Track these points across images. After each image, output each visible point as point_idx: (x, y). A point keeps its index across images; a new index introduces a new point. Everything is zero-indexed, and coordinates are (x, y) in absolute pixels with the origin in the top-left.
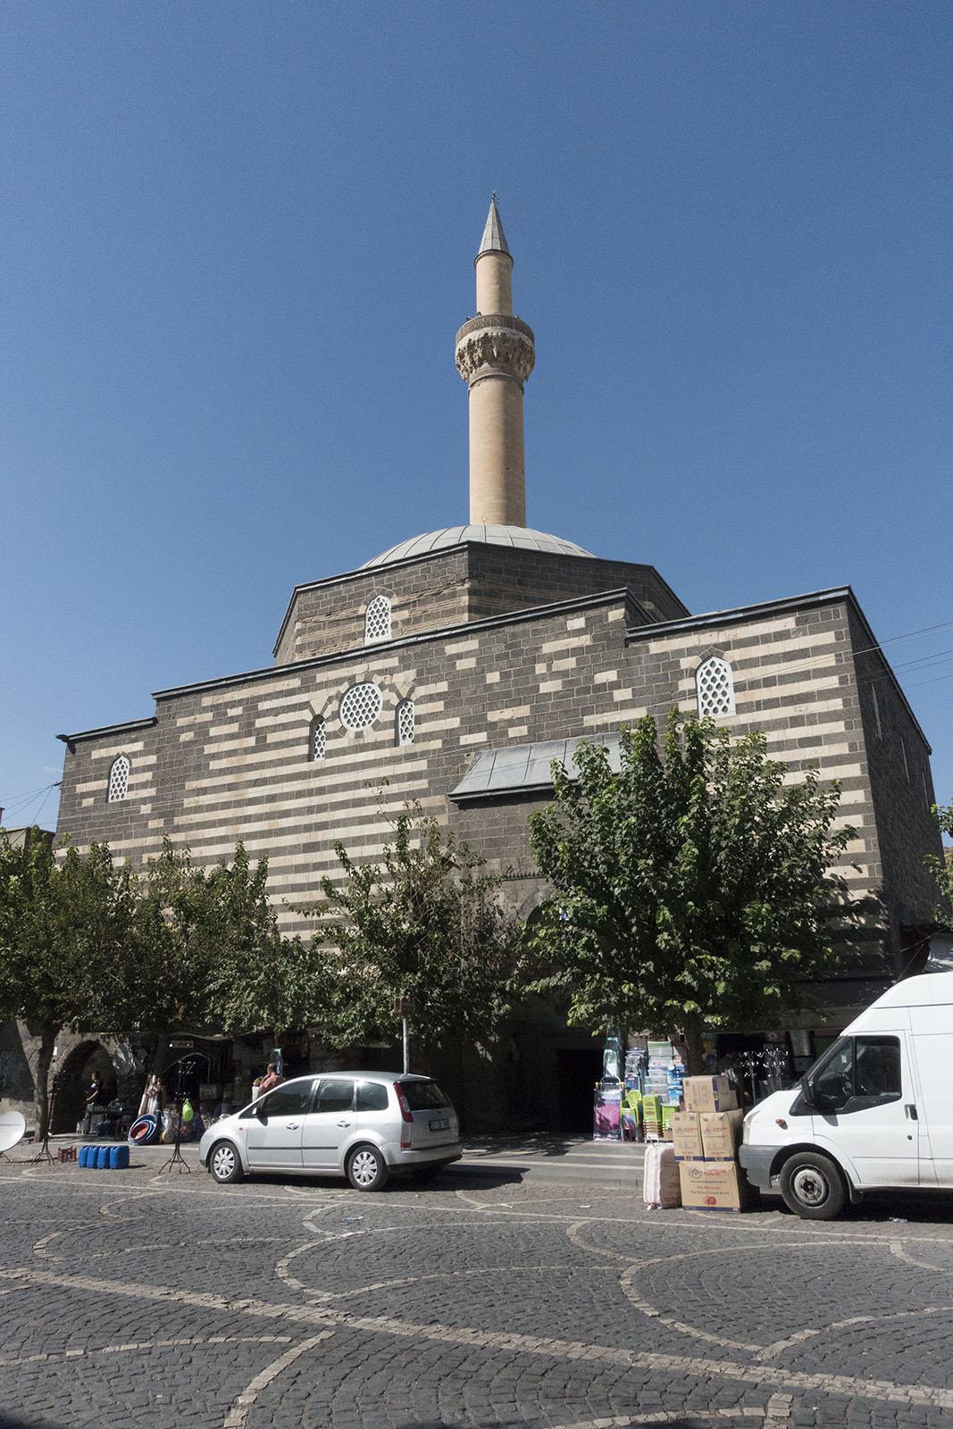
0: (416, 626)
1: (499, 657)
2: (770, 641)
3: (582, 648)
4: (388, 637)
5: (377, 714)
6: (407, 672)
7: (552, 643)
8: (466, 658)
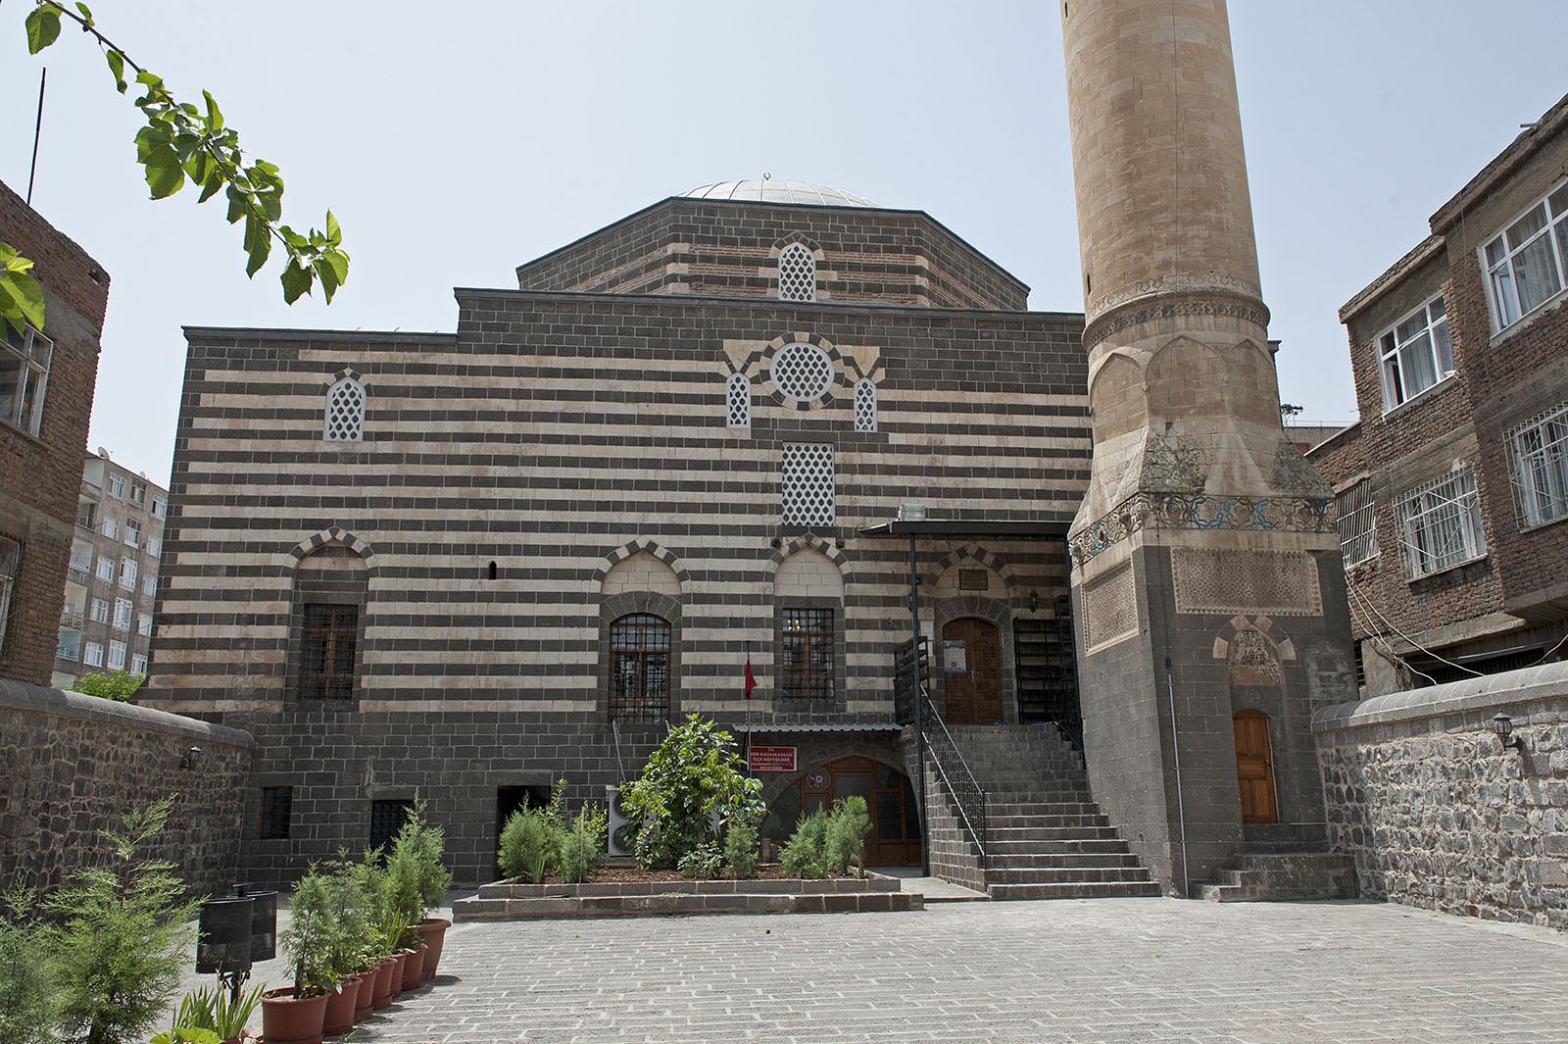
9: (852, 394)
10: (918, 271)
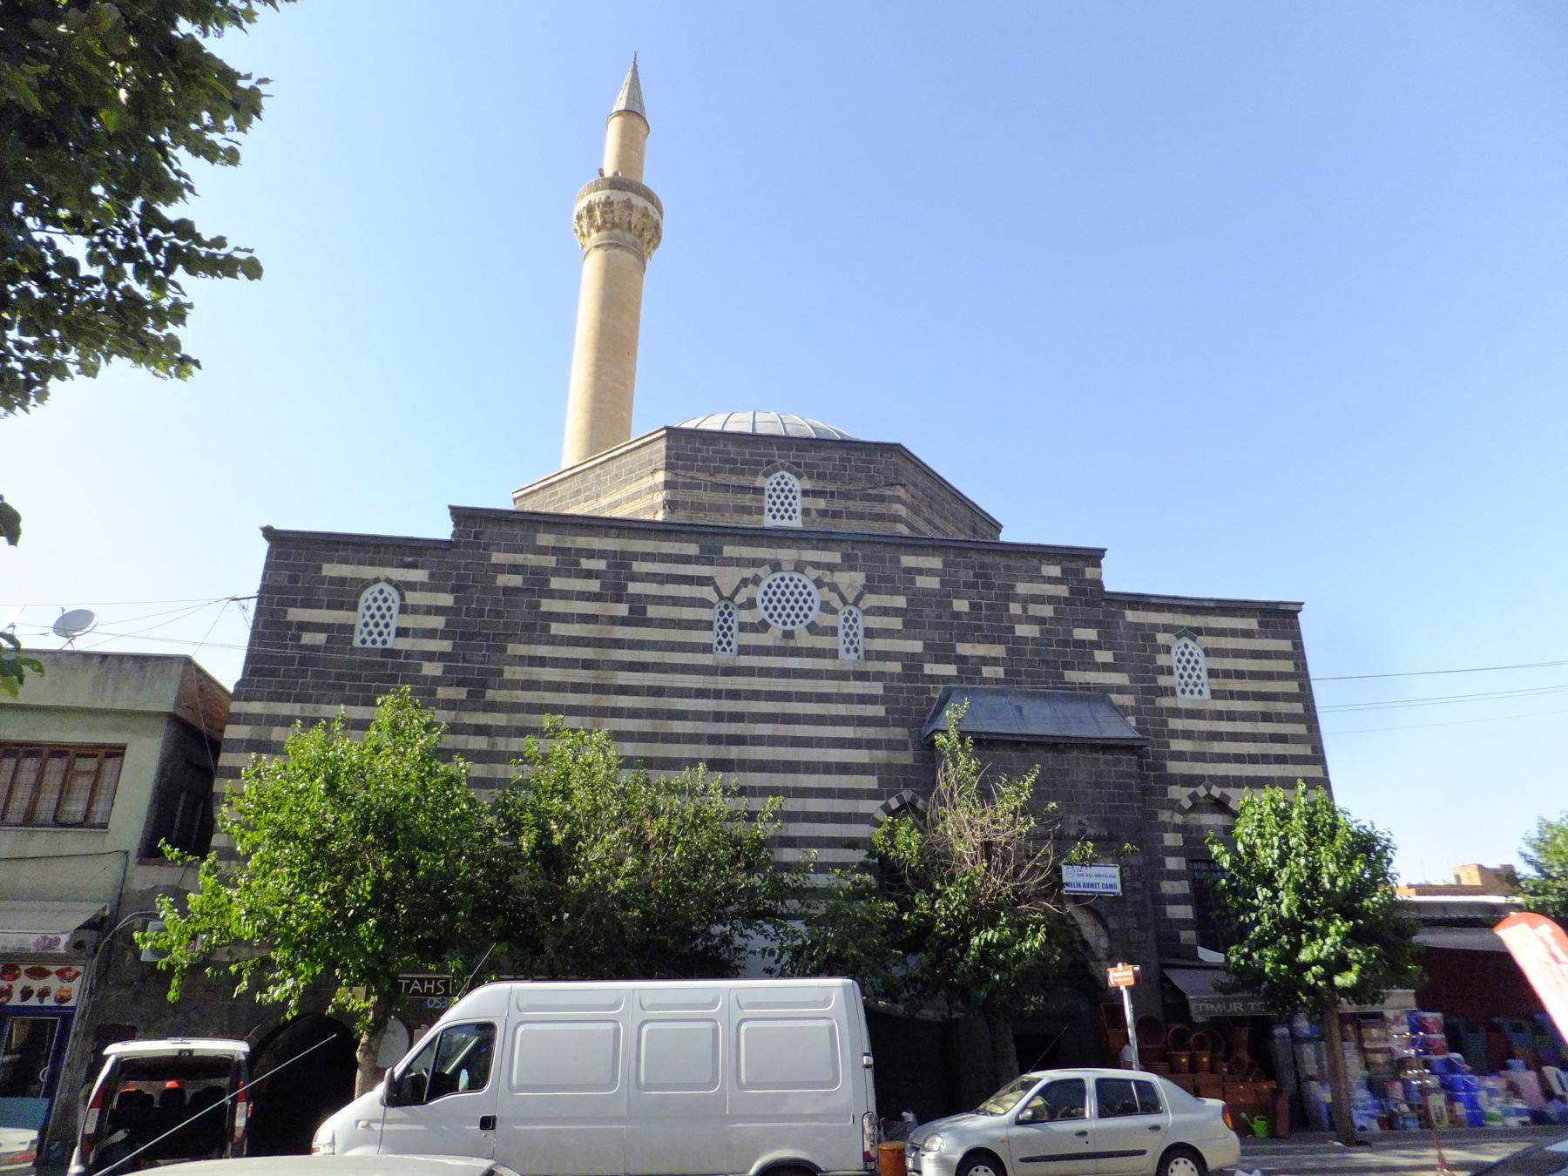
1: (968, 585)
4: (797, 523)
9: (838, 621)
10: (898, 499)
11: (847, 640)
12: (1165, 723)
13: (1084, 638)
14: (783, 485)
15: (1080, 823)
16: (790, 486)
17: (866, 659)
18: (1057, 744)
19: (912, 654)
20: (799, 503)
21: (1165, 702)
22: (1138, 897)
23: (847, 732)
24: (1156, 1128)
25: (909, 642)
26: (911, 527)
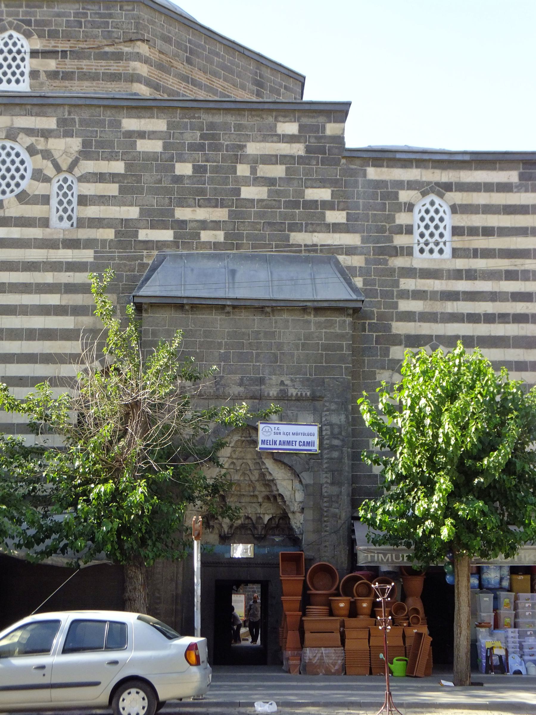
0: (67, 83)
1: (193, 147)
2: (492, 191)
3: (292, 157)
4: (24, 87)
5: (24, 184)
6: (68, 140)
7: (258, 144)
8: (149, 139)
10: (138, 57)
11: (61, 209)
12: (396, 284)
13: (316, 198)
14: (10, 46)
15: (282, 383)
16: (19, 46)
17: (78, 227)
18: (263, 307)
19: (126, 220)
20: (28, 65)
21: (399, 262)
22: (335, 454)
23: (53, 299)
24: (115, 663)
25: (124, 209)
26: (156, 87)
